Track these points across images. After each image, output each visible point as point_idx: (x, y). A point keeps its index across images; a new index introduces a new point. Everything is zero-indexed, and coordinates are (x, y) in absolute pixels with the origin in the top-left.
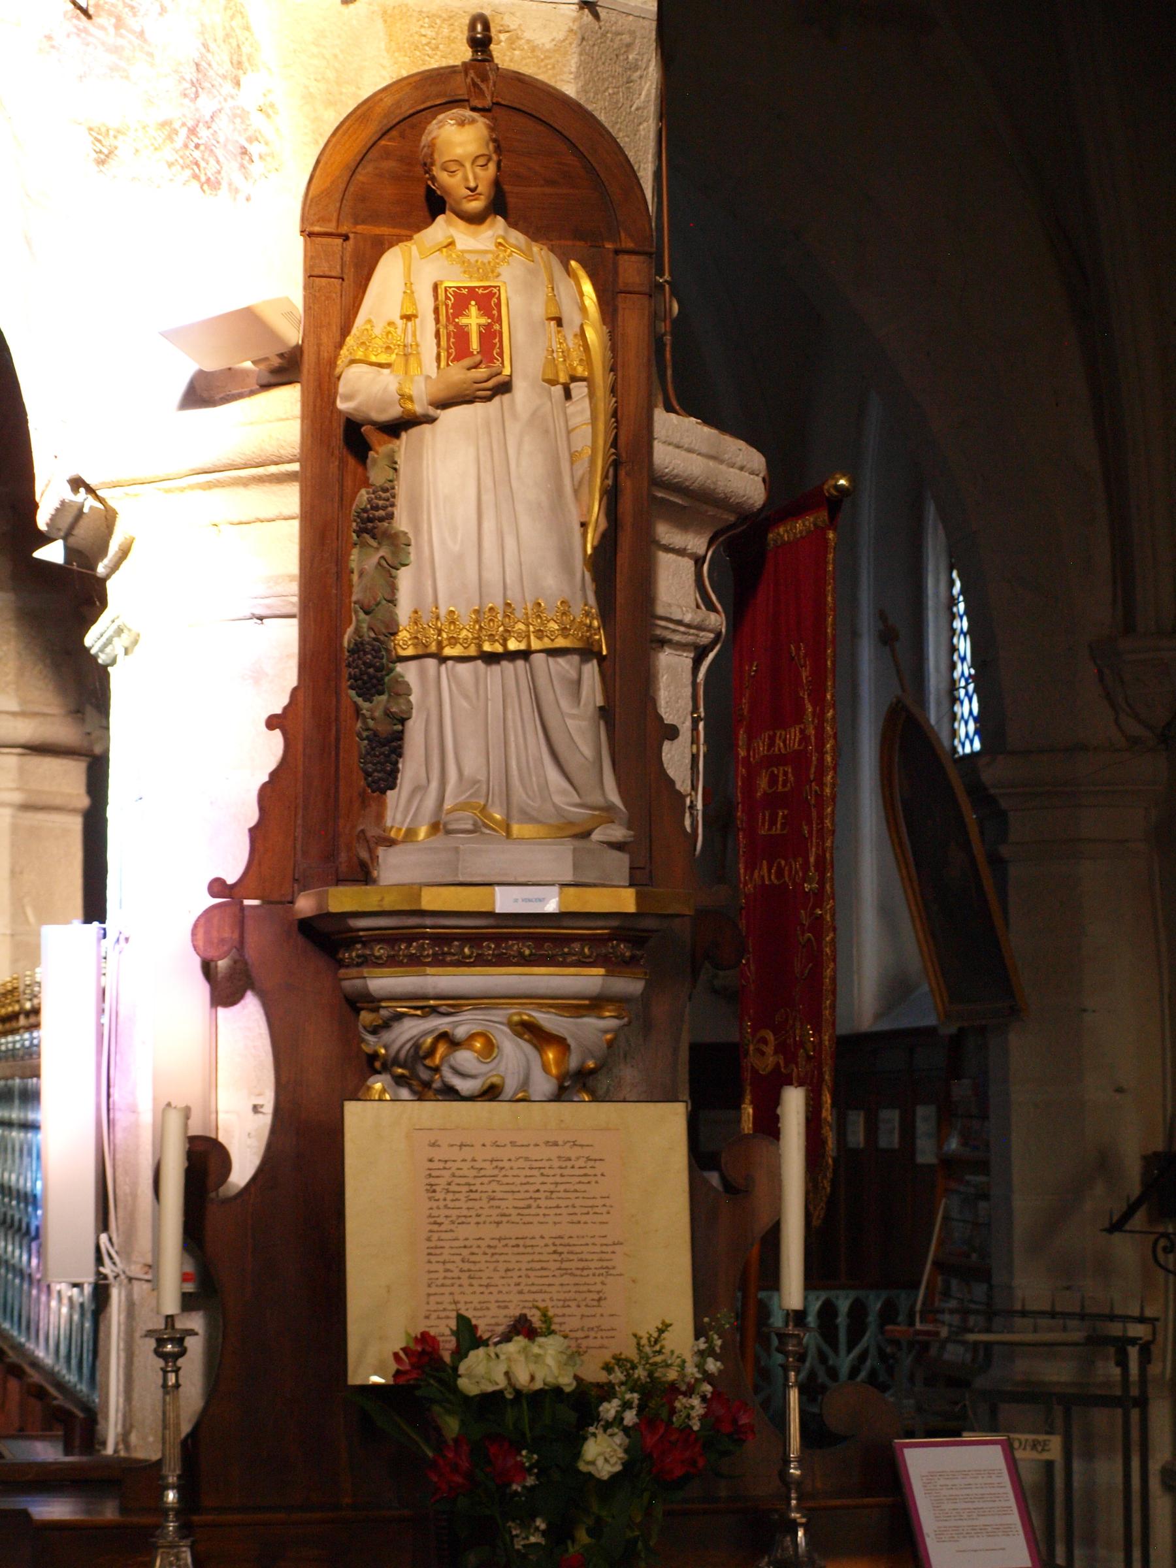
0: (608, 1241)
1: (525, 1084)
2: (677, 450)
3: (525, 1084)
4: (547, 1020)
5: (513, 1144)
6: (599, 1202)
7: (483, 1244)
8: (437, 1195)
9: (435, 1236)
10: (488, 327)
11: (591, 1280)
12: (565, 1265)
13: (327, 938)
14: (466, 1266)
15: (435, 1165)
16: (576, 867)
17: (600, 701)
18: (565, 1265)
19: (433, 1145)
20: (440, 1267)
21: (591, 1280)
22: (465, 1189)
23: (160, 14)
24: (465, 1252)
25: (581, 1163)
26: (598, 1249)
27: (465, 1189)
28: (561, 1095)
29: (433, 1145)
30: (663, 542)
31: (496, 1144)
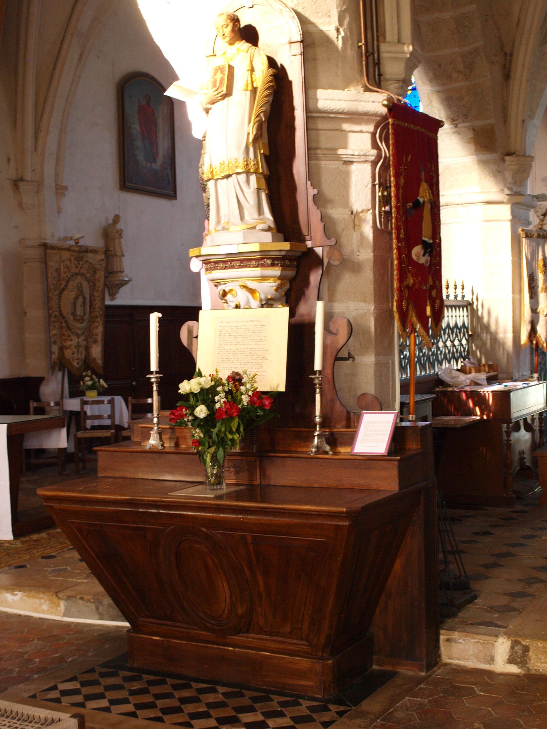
0: (265, 349)
1: (248, 302)
2: (333, 101)
3: (248, 302)
4: (252, 285)
5: (242, 321)
6: (263, 338)
7: (232, 351)
8: (222, 337)
9: (220, 348)
10: (222, 77)
11: (259, 361)
12: (253, 357)
13: (539, 236)
14: (227, 357)
15: (221, 328)
16: (244, 238)
17: (256, 187)
18: (253, 357)
19: (221, 322)
20: (220, 357)
21: (259, 361)
22: (228, 335)
23: (235, 20)
24: (227, 353)
25: (259, 326)
26: (262, 352)
27: (228, 335)
28: (262, 306)
29: (221, 322)
30: (348, 130)
31: (237, 322)
